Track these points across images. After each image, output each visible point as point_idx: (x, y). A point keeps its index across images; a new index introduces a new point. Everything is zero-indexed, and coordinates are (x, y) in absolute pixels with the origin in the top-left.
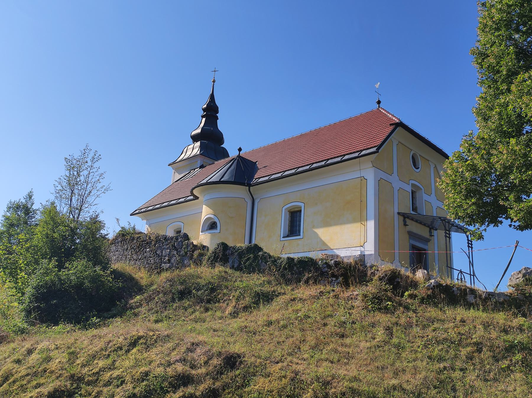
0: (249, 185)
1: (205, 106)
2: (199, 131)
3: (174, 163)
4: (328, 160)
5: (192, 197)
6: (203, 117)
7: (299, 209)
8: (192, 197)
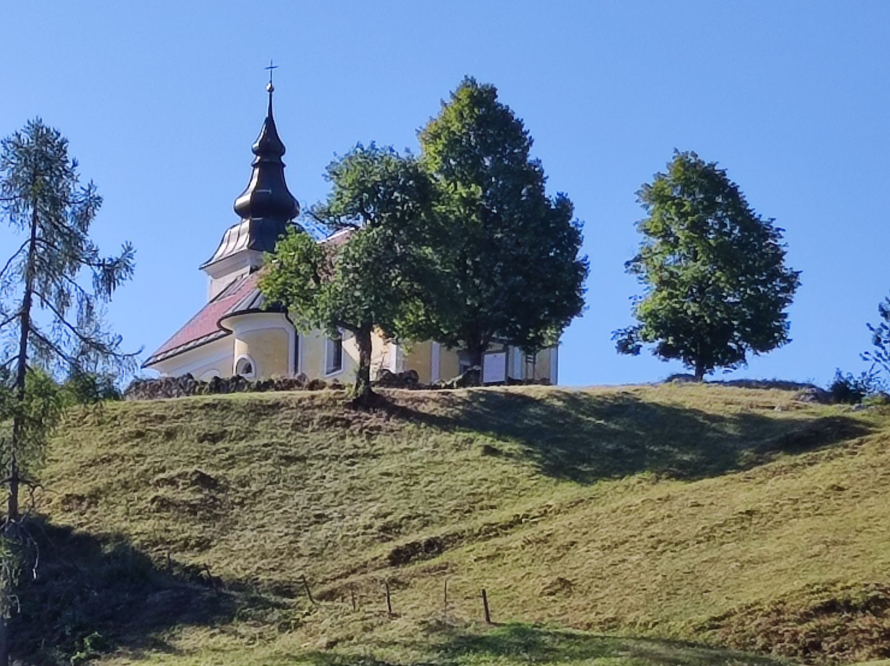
1: (257, 144)
2: (247, 198)
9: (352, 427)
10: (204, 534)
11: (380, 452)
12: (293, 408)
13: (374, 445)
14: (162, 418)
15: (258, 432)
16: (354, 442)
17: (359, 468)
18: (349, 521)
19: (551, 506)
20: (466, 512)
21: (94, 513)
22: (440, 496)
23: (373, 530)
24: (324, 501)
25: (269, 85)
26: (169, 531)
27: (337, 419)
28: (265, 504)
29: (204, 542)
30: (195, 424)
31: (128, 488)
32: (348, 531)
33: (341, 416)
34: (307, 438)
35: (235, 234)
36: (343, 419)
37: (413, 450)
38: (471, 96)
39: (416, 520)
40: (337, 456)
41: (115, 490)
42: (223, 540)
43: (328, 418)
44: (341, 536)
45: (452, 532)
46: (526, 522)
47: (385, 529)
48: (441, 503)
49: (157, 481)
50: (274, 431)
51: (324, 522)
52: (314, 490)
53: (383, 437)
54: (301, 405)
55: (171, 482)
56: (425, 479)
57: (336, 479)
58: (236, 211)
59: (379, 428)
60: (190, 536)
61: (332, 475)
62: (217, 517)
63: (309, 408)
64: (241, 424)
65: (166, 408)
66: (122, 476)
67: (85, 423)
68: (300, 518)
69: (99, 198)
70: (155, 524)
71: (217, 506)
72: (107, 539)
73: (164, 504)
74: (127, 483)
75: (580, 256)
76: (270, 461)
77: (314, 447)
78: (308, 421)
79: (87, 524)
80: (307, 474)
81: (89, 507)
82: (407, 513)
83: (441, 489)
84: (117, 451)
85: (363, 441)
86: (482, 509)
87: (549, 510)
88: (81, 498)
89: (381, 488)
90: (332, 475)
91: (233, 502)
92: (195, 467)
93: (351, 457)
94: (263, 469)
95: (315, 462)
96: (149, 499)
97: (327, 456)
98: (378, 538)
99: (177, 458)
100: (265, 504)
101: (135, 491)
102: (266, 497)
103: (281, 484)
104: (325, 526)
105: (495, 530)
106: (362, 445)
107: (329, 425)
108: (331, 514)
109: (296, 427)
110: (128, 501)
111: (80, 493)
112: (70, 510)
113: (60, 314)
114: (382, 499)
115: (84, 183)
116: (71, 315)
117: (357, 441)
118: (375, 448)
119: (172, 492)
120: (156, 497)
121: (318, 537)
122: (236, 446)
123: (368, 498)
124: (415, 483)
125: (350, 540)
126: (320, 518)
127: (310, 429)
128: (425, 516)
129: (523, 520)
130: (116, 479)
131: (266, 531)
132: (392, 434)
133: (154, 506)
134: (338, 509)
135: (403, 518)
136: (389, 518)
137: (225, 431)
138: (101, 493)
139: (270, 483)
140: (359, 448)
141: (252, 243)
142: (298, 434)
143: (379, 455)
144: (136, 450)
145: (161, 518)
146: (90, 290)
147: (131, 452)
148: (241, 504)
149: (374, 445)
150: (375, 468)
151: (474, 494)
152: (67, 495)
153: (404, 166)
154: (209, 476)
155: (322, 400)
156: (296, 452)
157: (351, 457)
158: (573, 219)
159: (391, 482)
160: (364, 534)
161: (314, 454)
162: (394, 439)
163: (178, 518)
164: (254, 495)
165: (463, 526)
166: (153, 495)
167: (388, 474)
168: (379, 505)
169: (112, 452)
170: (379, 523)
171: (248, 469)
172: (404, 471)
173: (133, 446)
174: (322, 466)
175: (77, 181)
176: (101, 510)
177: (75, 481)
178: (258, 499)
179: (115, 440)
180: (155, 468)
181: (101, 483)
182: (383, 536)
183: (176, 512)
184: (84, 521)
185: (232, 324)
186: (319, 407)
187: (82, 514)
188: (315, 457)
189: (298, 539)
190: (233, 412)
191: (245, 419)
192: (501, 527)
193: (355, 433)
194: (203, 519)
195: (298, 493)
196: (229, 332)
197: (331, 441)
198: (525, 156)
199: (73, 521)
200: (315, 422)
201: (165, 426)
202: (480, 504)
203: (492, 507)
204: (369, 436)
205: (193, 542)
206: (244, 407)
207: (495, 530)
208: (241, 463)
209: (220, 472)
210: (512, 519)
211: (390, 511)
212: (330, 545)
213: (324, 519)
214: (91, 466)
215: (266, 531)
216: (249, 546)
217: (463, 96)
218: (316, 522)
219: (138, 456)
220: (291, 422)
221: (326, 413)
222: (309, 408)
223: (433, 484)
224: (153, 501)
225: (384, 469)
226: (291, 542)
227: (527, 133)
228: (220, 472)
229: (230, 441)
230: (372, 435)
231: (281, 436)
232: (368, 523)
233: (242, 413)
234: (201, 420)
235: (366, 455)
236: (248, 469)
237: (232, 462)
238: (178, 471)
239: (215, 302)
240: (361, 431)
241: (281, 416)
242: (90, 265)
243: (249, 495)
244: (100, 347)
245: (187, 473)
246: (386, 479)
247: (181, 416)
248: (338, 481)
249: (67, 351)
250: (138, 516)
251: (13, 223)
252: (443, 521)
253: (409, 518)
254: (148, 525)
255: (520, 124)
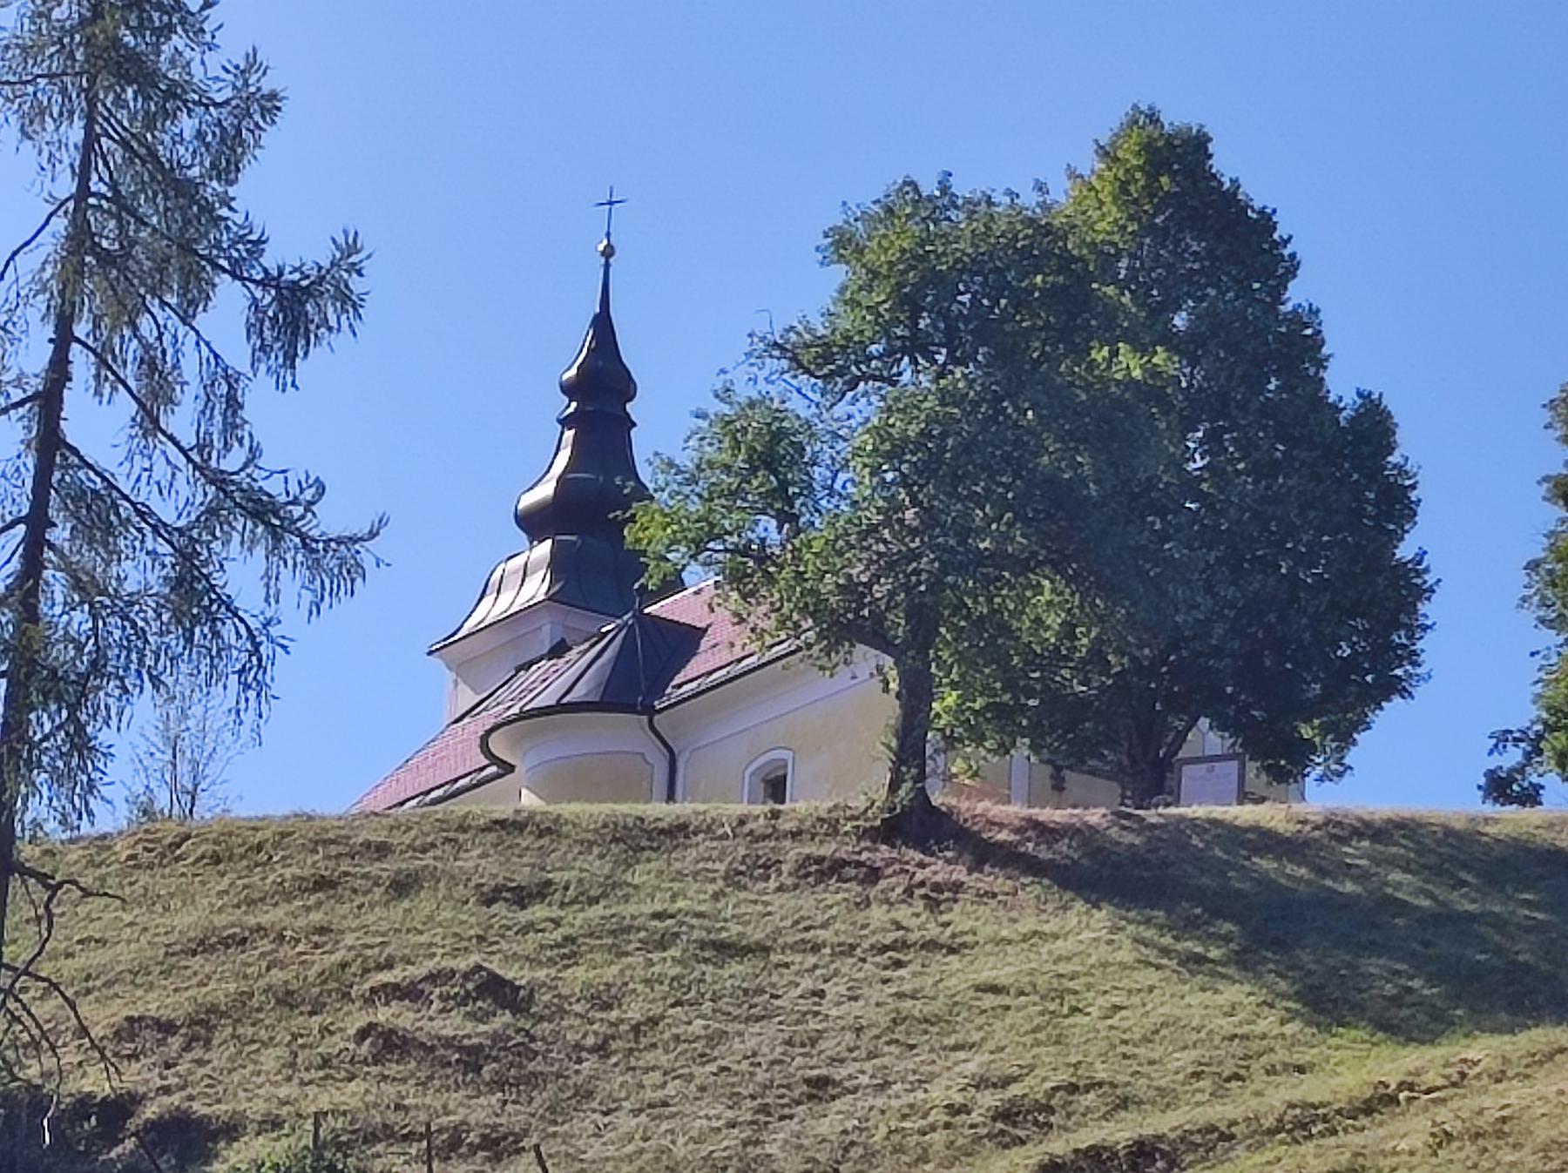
0: (651, 711)
1: (574, 371)
2: (546, 490)
3: (448, 642)
4: (456, 780)
5: (494, 769)
6: (565, 422)
7: (780, 773)
8: (494, 769)
9: (883, 884)
10: (503, 1120)
11: (969, 939)
12: (725, 837)
13: (947, 925)
14: (383, 850)
15: (636, 887)
16: (894, 915)
17: (914, 974)
18: (897, 1097)
19: (1476, 1063)
20: (1228, 1080)
21: (200, 1063)
22: (1147, 1040)
23: (975, 1117)
24: (828, 1045)
25: (605, 242)
26: (406, 1109)
27: (845, 863)
28: (667, 1052)
29: (505, 1138)
30: (471, 864)
31: (292, 1007)
32: (904, 1117)
33: (856, 857)
34: (766, 904)
35: (516, 572)
36: (859, 864)
37: (1056, 937)
38: (1148, 148)
39: (1092, 1096)
40: (853, 947)
41: (259, 1010)
42: (555, 1134)
43: (819, 860)
44: (883, 1130)
45: (1201, 1123)
46: (1409, 1100)
47: (1006, 1114)
48: (1155, 1056)
49: (373, 990)
50: (676, 886)
51: (833, 1098)
52: (798, 1022)
53: (969, 908)
54: (746, 829)
55: (409, 993)
56: (1101, 1001)
57: (856, 999)
58: (516, 516)
59: (957, 887)
60: (463, 1123)
61: (842, 989)
62: (534, 1080)
63: (765, 837)
64: (597, 866)
65: (392, 828)
66: (277, 976)
67: (177, 859)
68: (767, 1086)
69: (273, 96)
70: (367, 1091)
71: (536, 1053)
72: (235, 1128)
73: (391, 1044)
74: (290, 993)
75: (1405, 551)
76: (674, 952)
77: (788, 923)
78: (766, 867)
79: (183, 1088)
80: (773, 985)
81: (187, 1048)
82: (1064, 1077)
83: (1149, 1023)
84: (265, 920)
85: (918, 915)
86: (1273, 1070)
87: (1472, 1073)
88: (168, 1028)
89: (981, 1020)
90: (842, 989)
91: (578, 1047)
92: (474, 959)
93: (886, 948)
94: (657, 969)
95: (798, 958)
96: (352, 1032)
97: (824, 945)
98: (989, 1136)
99: (423, 939)
100: (667, 1052)
101: (312, 1013)
102: (666, 1036)
103: (707, 1006)
104: (838, 1105)
105: (1325, 1119)
106: (915, 922)
107: (822, 876)
108: (850, 1077)
109: (733, 878)
110: (295, 1037)
111: (166, 1014)
112: (134, 1056)
113: (149, 423)
114: (991, 1045)
115: (232, 50)
116: (182, 421)
117: (902, 913)
118: (948, 931)
119: (411, 1015)
120: (372, 1026)
121: (819, 1130)
122: (581, 915)
123: (950, 1041)
124: (1075, 1010)
125: (912, 1141)
126: (820, 1090)
127: (772, 884)
128: (1113, 1085)
129: (1402, 1096)
130: (262, 983)
131: (673, 1115)
132: (993, 903)
133: (365, 1048)
134: (868, 1066)
135: (1055, 1089)
136: (1015, 1090)
137: (549, 883)
138: (223, 1015)
139: (678, 1003)
140: (907, 930)
141: (556, 588)
142: (743, 895)
143: (964, 945)
144: (316, 917)
145: (385, 1078)
146: (237, 354)
147: (301, 922)
148: (602, 1049)
149: (947, 925)
150: (958, 974)
151: (1245, 1037)
152: (130, 1019)
153: (1031, 222)
154: (510, 983)
155: (801, 821)
156: (742, 935)
157: (886, 948)
158: (1394, 459)
159: (1007, 1008)
160: (947, 1126)
161: (790, 940)
162: (1001, 913)
163: (430, 1078)
164: (636, 1029)
165: (1219, 1113)
166: (361, 1020)
167: (995, 989)
168: (987, 1057)
169: (252, 921)
170: (990, 1099)
171: (615, 969)
172: (1041, 981)
173: (308, 909)
174: (816, 967)
175: (211, 47)
176: (219, 1057)
177: (151, 986)
178: (644, 1041)
179: (257, 895)
180: (366, 959)
181: (222, 991)
182: (1002, 1133)
183: (425, 1066)
184: (175, 1081)
185: (514, 744)
186: (795, 835)
187: (168, 1066)
188: (793, 947)
189: (765, 1136)
190: (565, 842)
191: (601, 857)
192: (1339, 1112)
193: (893, 896)
194: (499, 1084)
195: (756, 1028)
196: (510, 768)
197: (834, 911)
198: (1278, 299)
199: (147, 1081)
200: (785, 868)
201: (387, 868)
202: (1264, 1059)
203: (1301, 1069)
204: (933, 905)
205: (473, 1138)
206: (596, 831)
207: (1325, 1119)
208: (598, 957)
209: (541, 974)
210: (1368, 1093)
211: (1016, 1071)
212: (856, 1152)
213: (832, 1091)
214: (194, 953)
215: (673, 1115)
216: (630, 1148)
217: (1129, 154)
218: (811, 1097)
219: (322, 930)
220: (722, 867)
221: (812, 849)
222: (765, 837)
223: (1124, 1013)
224: (363, 1034)
225: (985, 976)
226: (745, 1144)
227: (1286, 242)
228: (541, 974)
229: (562, 905)
230: (939, 903)
231: (695, 898)
232: (958, 1099)
233: (591, 844)
234: (484, 855)
235: (931, 945)
236: (615, 969)
237: (570, 951)
238: (429, 966)
239: (466, 720)
240: (909, 892)
241: (692, 854)
242: (242, 279)
243: (624, 1028)
244: (261, 509)
245: (453, 972)
246: (989, 1000)
247: (433, 845)
248: (861, 1003)
249: (166, 512)
250: (321, 1074)
251: (29, 143)
252: (1166, 1098)
253: (1073, 1089)
254: (351, 1094)
255: (1266, 222)
